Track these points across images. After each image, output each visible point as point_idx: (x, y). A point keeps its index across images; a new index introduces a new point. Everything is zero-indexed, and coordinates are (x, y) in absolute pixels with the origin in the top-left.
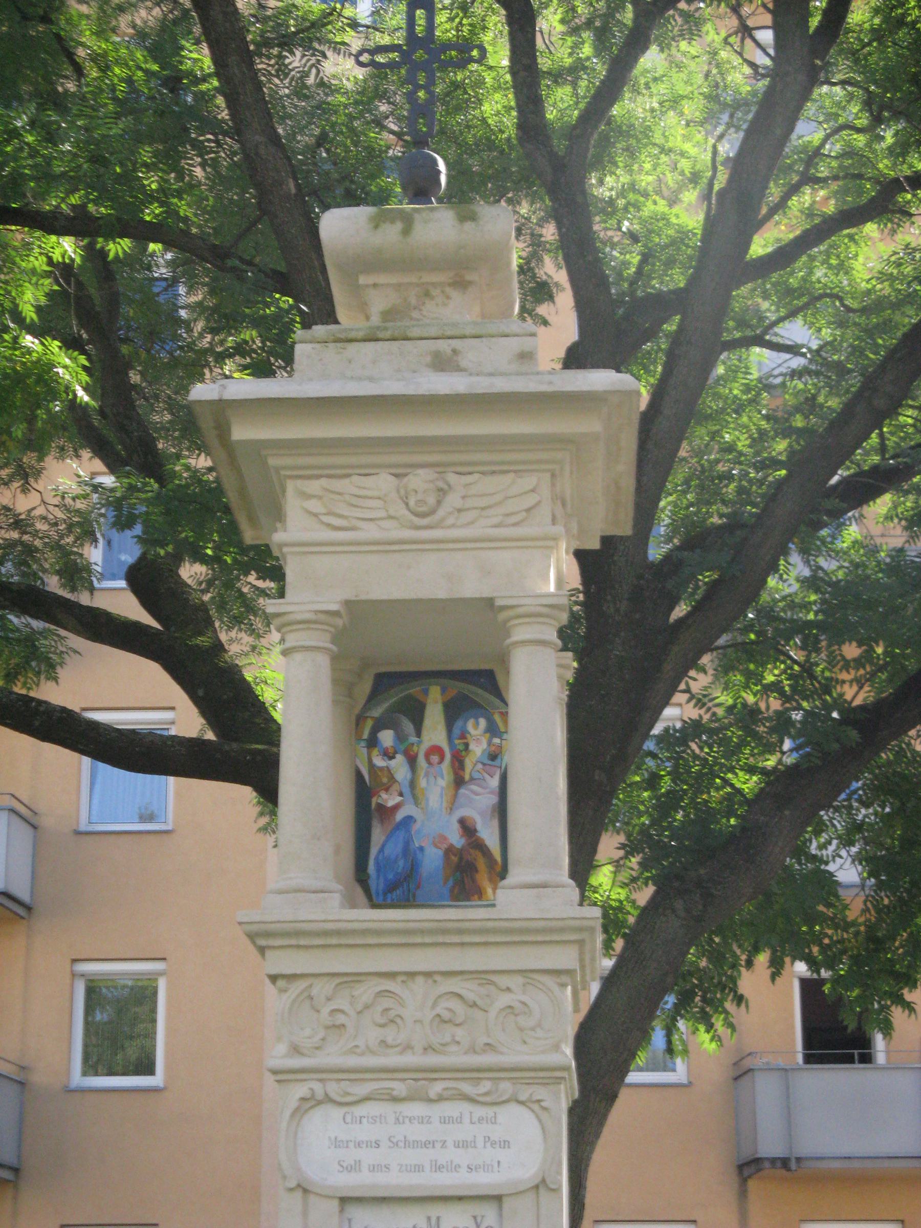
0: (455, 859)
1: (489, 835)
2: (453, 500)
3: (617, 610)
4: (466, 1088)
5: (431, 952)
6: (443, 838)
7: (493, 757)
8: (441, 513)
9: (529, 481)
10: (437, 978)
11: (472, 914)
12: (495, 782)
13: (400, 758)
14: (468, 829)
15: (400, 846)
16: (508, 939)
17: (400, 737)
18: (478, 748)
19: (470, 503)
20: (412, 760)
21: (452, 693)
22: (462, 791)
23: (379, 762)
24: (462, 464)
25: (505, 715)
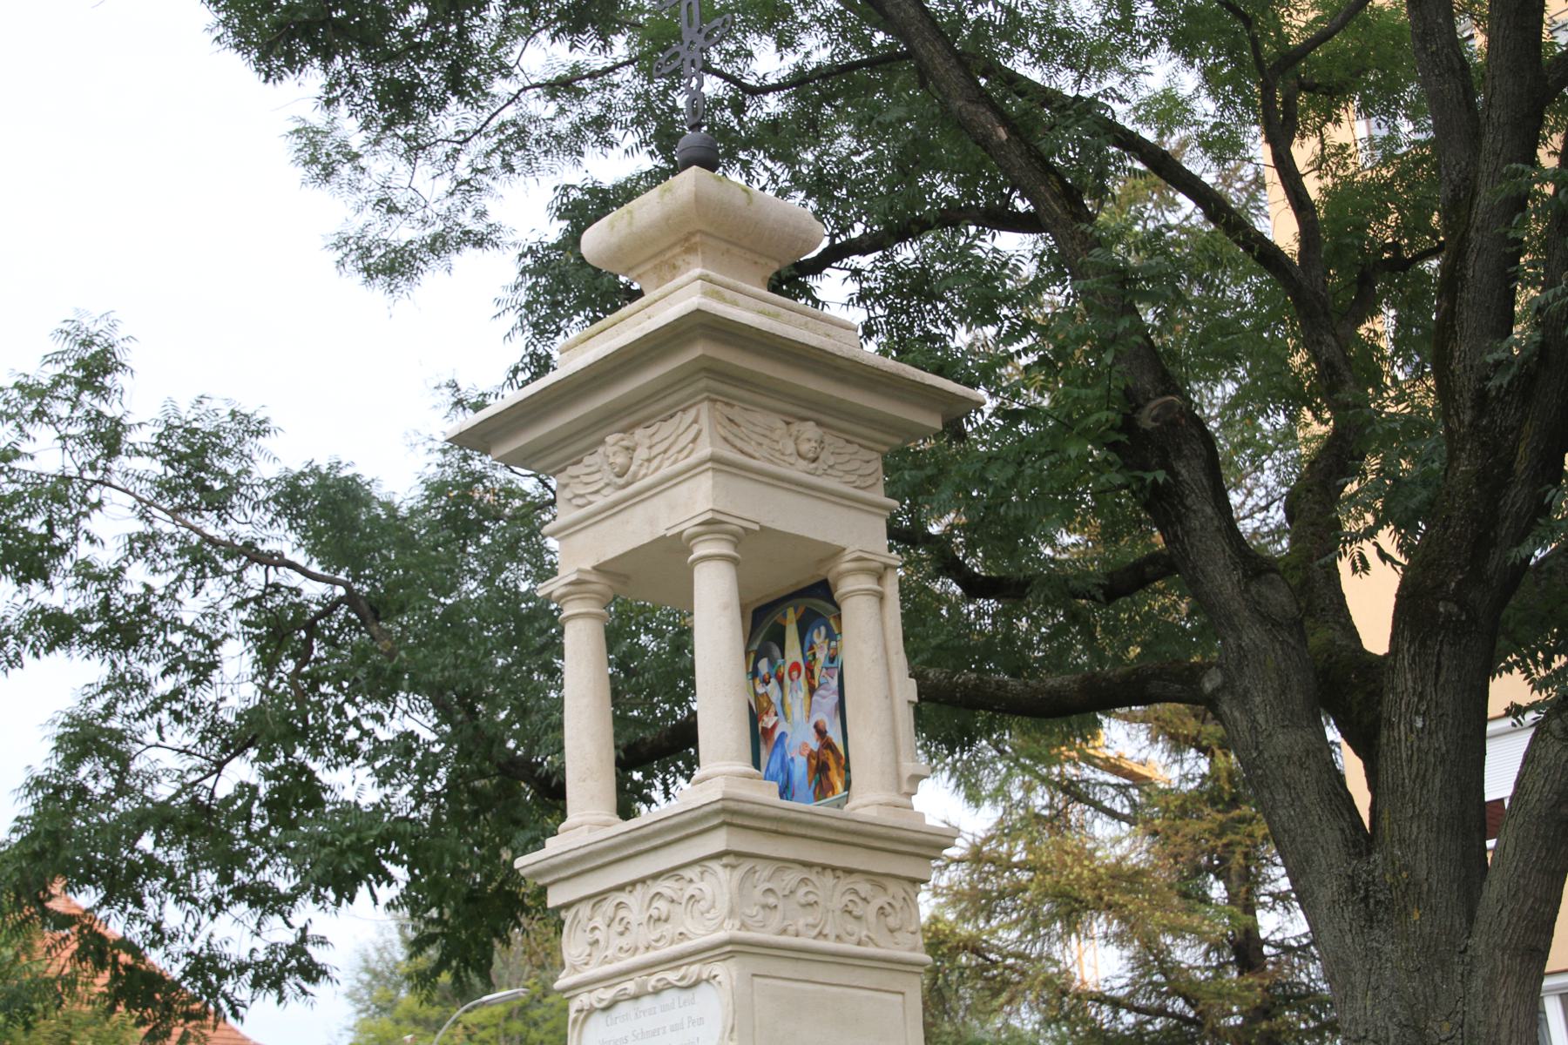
0: (814, 762)
1: (834, 735)
2: (641, 454)
3: (1461, 423)
4: (672, 976)
5: (652, 857)
6: (805, 744)
7: (832, 659)
8: (633, 468)
9: (692, 413)
10: (839, 873)
11: (821, 808)
12: (834, 683)
13: (773, 681)
14: (821, 732)
15: (778, 765)
16: (683, 833)
17: (772, 663)
18: (822, 656)
19: (655, 451)
20: (781, 681)
21: (801, 609)
22: (815, 698)
23: (760, 690)
24: (660, 413)
25: (839, 618)
